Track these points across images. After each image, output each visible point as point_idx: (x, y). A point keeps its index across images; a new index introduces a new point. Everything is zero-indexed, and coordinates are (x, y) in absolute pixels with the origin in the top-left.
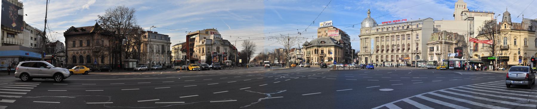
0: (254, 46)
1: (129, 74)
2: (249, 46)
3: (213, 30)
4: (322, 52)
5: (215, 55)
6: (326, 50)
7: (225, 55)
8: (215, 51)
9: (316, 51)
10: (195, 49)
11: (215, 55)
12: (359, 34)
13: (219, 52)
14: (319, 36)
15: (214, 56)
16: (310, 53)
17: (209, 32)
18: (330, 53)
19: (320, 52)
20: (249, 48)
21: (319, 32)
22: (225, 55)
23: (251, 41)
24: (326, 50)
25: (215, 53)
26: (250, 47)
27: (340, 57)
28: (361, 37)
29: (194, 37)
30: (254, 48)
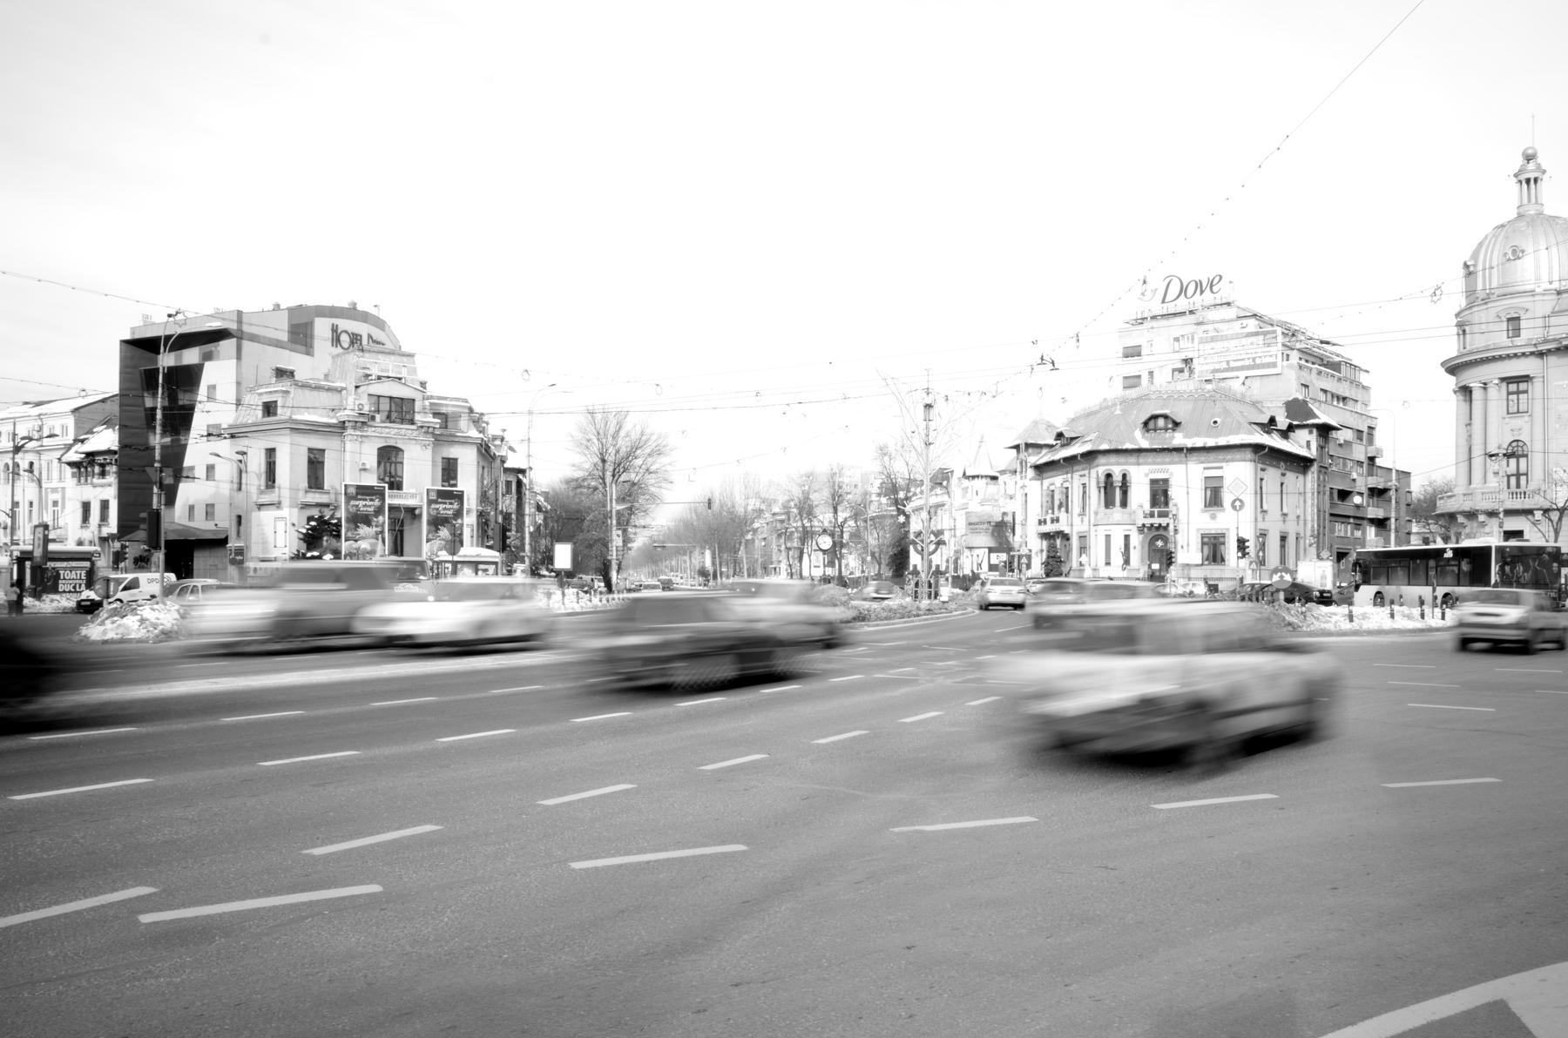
0: (658, 452)
1: (543, 728)
2: (624, 445)
3: (352, 313)
4: (1160, 494)
5: (366, 505)
6: (1187, 480)
7: (446, 509)
8: (371, 480)
9: (1114, 492)
10: (197, 452)
11: (366, 505)
12: (1451, 348)
13: (396, 485)
14: (1132, 382)
15: (358, 519)
16: (1065, 505)
17: (322, 327)
18: (1214, 498)
19: (1140, 495)
20: (620, 467)
21: (1133, 353)
22: (446, 509)
23: (632, 426)
24: (1187, 480)
25: (364, 491)
26: (631, 454)
27: (1292, 529)
28: (1473, 378)
29: (191, 356)
30: (657, 463)
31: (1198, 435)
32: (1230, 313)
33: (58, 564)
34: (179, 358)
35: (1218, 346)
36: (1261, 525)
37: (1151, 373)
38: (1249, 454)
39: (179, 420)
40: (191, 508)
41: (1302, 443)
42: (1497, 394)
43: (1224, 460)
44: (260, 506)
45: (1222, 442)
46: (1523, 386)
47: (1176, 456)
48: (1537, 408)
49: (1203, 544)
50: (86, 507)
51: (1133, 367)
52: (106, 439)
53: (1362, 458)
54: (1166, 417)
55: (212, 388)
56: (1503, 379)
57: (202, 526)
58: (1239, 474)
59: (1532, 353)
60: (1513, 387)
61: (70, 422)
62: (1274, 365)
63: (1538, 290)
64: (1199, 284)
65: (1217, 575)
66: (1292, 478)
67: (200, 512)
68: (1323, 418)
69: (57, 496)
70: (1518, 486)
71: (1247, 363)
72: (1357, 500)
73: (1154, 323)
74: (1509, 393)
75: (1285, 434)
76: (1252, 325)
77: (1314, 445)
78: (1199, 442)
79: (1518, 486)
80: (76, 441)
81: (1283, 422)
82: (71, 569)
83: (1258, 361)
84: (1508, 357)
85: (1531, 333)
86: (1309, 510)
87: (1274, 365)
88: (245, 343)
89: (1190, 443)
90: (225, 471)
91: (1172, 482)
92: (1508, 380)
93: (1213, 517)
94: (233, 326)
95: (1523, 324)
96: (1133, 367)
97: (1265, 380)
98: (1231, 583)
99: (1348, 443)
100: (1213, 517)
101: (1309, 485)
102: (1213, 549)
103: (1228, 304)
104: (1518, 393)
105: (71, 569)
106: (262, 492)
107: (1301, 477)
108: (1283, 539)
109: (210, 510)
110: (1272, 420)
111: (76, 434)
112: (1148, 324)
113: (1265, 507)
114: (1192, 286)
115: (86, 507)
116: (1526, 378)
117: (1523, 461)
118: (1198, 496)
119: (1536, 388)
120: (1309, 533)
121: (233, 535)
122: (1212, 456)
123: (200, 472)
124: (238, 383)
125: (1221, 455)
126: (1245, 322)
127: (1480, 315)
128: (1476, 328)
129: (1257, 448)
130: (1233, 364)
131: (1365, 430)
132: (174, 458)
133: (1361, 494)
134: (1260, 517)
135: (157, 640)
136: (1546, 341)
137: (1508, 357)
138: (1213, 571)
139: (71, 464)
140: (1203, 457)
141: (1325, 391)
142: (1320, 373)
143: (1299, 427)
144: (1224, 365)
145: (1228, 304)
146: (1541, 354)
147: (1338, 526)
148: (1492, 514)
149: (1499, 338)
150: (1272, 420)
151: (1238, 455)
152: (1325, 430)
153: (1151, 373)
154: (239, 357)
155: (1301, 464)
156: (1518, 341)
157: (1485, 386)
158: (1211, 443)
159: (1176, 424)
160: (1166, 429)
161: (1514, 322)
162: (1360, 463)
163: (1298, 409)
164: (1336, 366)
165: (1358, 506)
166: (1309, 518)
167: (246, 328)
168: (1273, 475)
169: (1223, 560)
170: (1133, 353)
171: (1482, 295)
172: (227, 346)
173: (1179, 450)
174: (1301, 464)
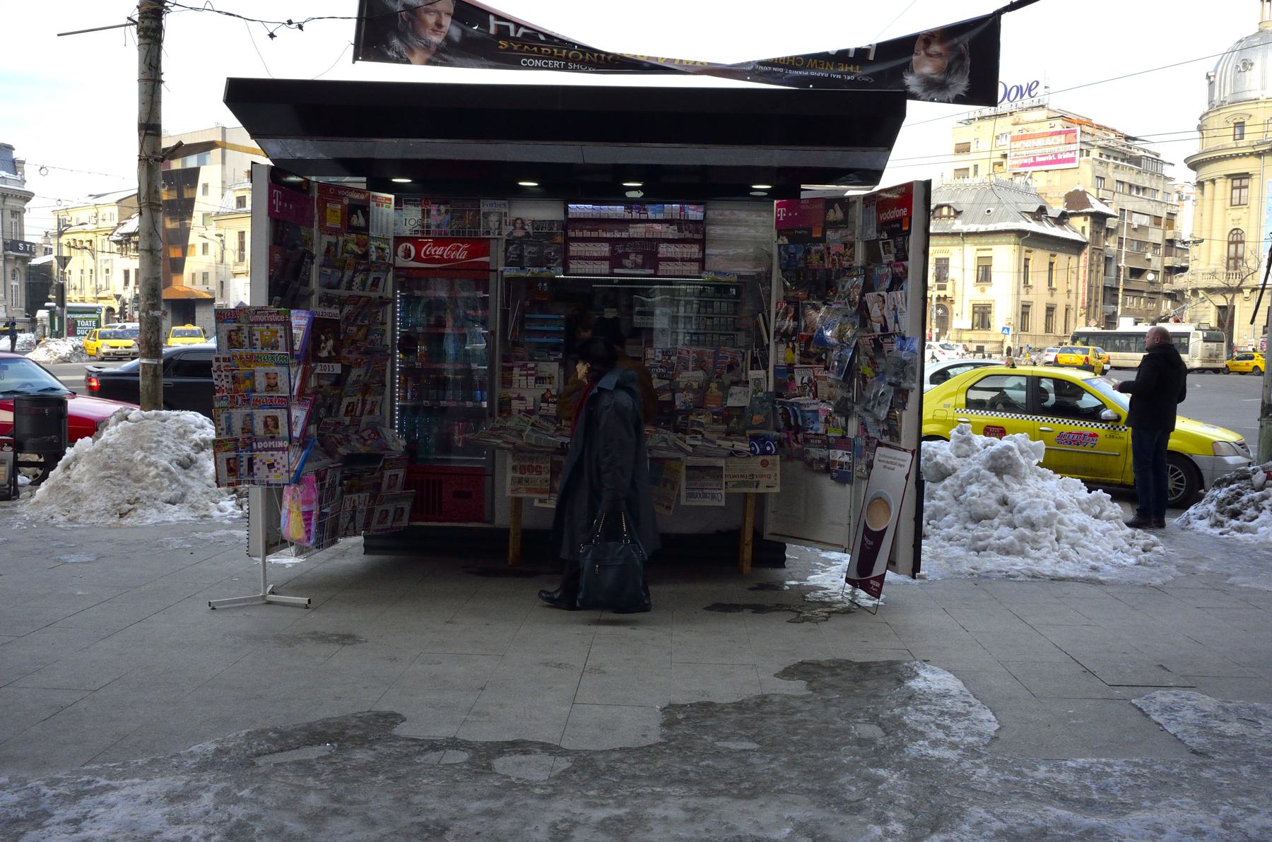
12: (1193, 147)
18: (984, 274)
21: (963, 149)
29: (192, 162)
31: (973, 222)
32: (1042, 114)
33: (76, 316)
34: (184, 163)
35: (1027, 143)
36: (1024, 297)
37: (976, 166)
38: (1013, 238)
39: (184, 208)
40: (194, 275)
41: (1079, 229)
42: (1223, 187)
43: (993, 243)
44: (235, 275)
45: (991, 228)
46: (1244, 182)
47: (957, 240)
48: (1254, 204)
49: (974, 312)
50: (127, 273)
51: (964, 161)
52: (133, 225)
53: (1159, 240)
54: (949, 207)
55: (206, 186)
56: (1228, 176)
57: (200, 290)
58: (1005, 256)
59: (1251, 154)
60: (1237, 183)
61: (115, 210)
62: (1072, 160)
63: (1262, 99)
64: (1019, 89)
65: (983, 338)
66: (1061, 259)
67: (199, 279)
68: (1098, 207)
69: (108, 266)
70: (1236, 268)
71: (1050, 158)
72: (1151, 277)
73: (982, 123)
74: (1233, 188)
75: (1062, 219)
76: (1059, 125)
77: (1088, 230)
78: (973, 228)
79: (1236, 268)
80: (119, 224)
81: (1056, 208)
82: (85, 319)
83: (1060, 157)
84: (1232, 157)
85: (1253, 135)
86: (1081, 285)
87: (1072, 160)
88: (228, 152)
89: (965, 229)
90: (214, 248)
91: (951, 264)
92: (1233, 177)
93: (983, 290)
94: (219, 139)
95: (1247, 130)
96: (964, 161)
97: (1065, 173)
98: (994, 345)
99: (1141, 228)
100: (983, 290)
101: (1082, 264)
102: (982, 316)
103: (1043, 106)
104: (1240, 188)
105: (85, 319)
106: (236, 264)
107: (1074, 258)
108: (1050, 310)
109: (205, 276)
110: (1042, 210)
111: (120, 219)
112: (975, 124)
113: (1030, 283)
114: (1014, 90)
115: (127, 273)
116: (1246, 176)
117: (1240, 246)
118: (971, 275)
119: (1254, 184)
120: (1080, 305)
121: (217, 296)
122: (983, 240)
123: (199, 249)
124: (223, 182)
125: (991, 239)
126: (1053, 122)
127: (1216, 121)
128: (1211, 134)
129: (1020, 233)
130: (1038, 159)
131: (1164, 215)
132: (180, 239)
133: (1155, 272)
134: (1023, 291)
135: (56, 362)
136: (1264, 143)
137: (1232, 157)
138: (980, 335)
139: (116, 242)
140: (977, 240)
141: (1123, 183)
142: (1117, 167)
143: (1073, 215)
144: (1031, 160)
145: (1043, 106)
146: (1259, 155)
147: (1129, 300)
148: (1210, 290)
149: (1227, 141)
150: (1042, 210)
151: (1004, 239)
152: (1099, 219)
153: (976, 166)
154: (223, 162)
155: (1075, 247)
156: (1241, 143)
157: (1213, 181)
158: (982, 228)
159: (958, 213)
160: (949, 217)
161: (1240, 125)
162: (1156, 246)
163: (1076, 200)
164: (1137, 161)
165: (1152, 283)
166: (1081, 292)
167: (228, 141)
168: (1039, 258)
169: (989, 326)
170: (963, 149)
171: (1217, 103)
172: (216, 153)
173: (955, 234)
174: (1075, 247)
